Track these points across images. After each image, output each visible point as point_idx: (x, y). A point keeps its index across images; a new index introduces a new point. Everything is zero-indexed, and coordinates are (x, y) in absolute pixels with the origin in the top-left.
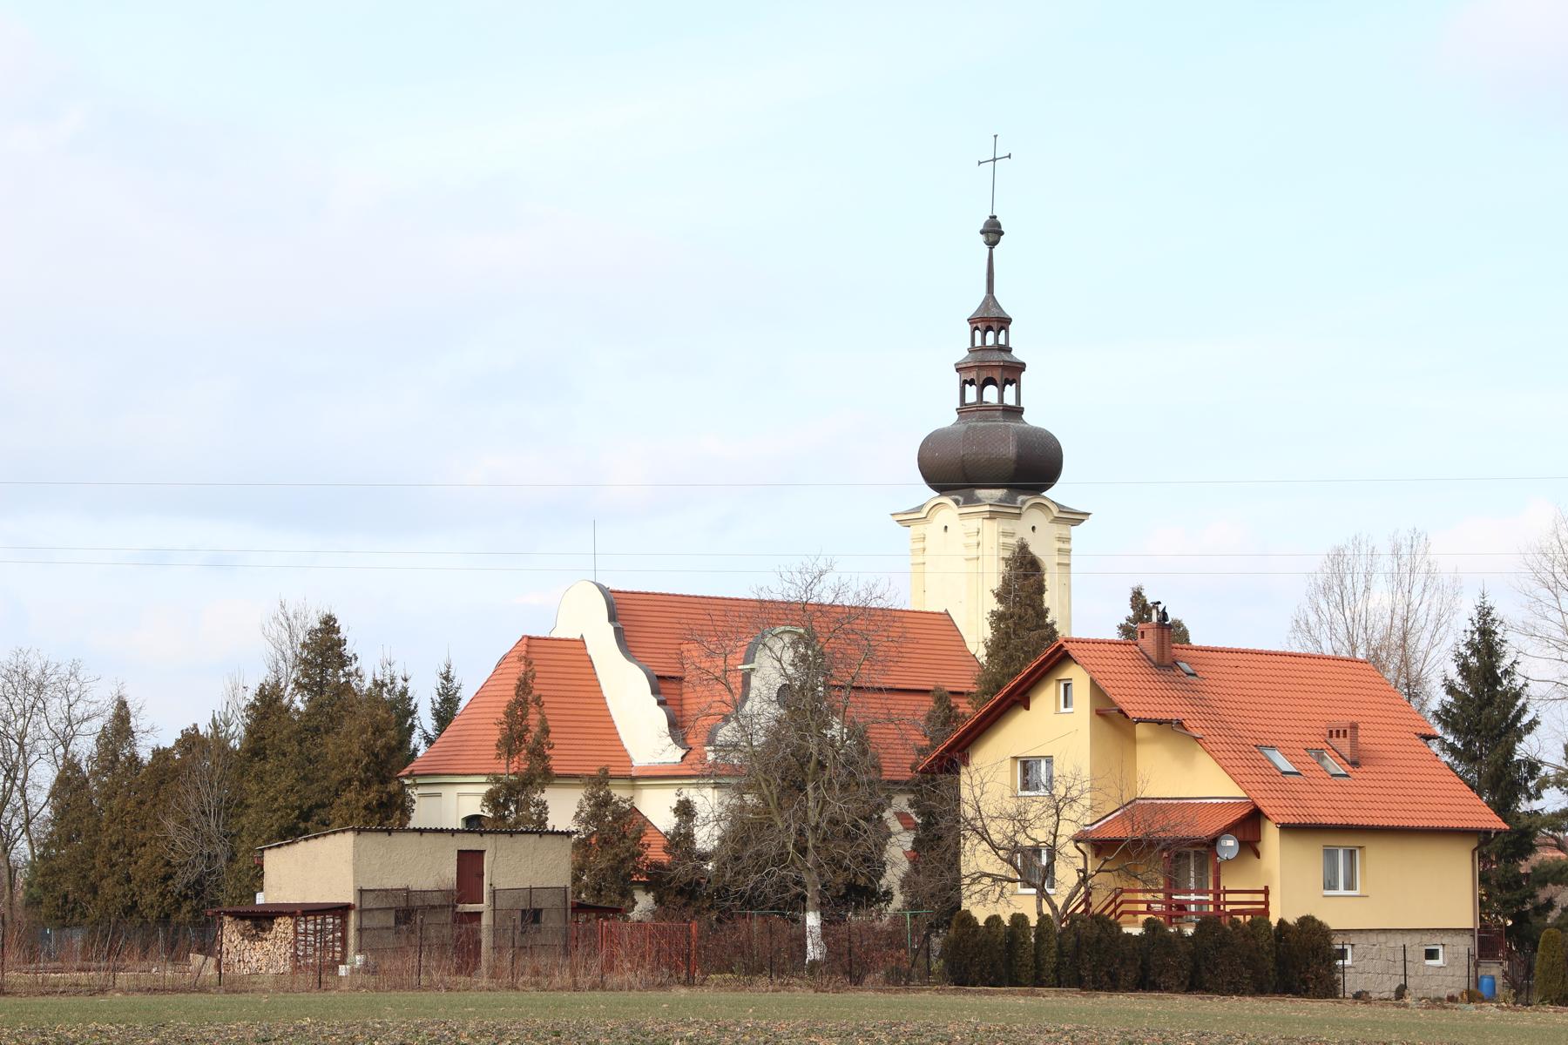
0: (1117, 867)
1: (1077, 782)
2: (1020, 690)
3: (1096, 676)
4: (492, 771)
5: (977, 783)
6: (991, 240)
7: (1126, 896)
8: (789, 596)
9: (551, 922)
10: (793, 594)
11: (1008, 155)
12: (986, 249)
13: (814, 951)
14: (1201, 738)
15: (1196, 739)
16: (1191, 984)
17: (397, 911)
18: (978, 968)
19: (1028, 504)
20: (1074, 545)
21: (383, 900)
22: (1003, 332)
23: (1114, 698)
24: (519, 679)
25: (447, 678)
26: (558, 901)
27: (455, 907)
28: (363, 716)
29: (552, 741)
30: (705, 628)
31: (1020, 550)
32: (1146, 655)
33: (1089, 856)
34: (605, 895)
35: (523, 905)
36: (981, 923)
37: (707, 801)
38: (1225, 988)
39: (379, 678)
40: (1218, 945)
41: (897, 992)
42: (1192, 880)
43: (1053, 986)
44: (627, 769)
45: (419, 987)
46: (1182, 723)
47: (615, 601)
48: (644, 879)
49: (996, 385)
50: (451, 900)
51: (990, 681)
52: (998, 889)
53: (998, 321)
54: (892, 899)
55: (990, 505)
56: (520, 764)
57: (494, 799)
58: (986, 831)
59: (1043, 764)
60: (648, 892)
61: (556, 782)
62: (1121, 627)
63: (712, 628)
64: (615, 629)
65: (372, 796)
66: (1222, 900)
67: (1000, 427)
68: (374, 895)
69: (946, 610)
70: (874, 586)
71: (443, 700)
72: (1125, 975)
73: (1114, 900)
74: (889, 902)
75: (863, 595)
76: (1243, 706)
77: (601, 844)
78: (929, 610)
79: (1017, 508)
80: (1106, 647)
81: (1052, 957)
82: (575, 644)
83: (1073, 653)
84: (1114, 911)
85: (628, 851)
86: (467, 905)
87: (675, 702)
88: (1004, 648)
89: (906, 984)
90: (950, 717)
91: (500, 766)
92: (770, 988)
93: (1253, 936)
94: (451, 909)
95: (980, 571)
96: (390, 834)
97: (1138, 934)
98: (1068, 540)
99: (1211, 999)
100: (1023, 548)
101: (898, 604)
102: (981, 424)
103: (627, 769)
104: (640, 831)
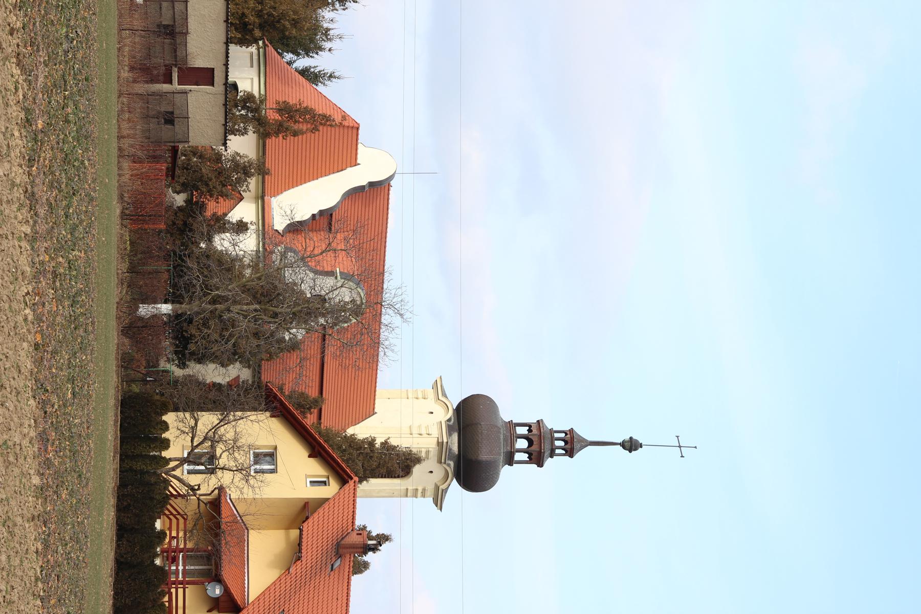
0: (201, 512)
1: (259, 483)
2: (322, 452)
3: (331, 501)
4: (268, 98)
5: (259, 418)
6: (626, 444)
7: (181, 521)
8: (386, 294)
9: (166, 132)
10: (387, 297)
11: (683, 455)
12: (620, 441)
13: (144, 310)
14: (289, 573)
15: (289, 569)
16: (122, 563)
17: (173, 26)
18: (133, 415)
19: (448, 469)
20: (420, 499)
21: (180, 16)
22: (564, 452)
23: (316, 514)
24: (330, 116)
25: (331, 76)
26: (180, 137)
27: (176, 65)
28: (305, 13)
29: (288, 138)
30: (365, 236)
31: (416, 458)
32: (345, 536)
33: (208, 497)
34: (184, 172)
35: (177, 112)
36: (164, 418)
37: (249, 243)
38: (119, 586)
39: (331, 32)
40: (148, 581)
41: (117, 359)
42: (192, 567)
43: (120, 467)
44: (269, 194)
45: (121, 30)
46: (299, 560)
47: (383, 186)
48: (194, 200)
49: (528, 447)
50: (180, 63)
51: (328, 437)
52: (187, 430)
53: (571, 448)
54: (181, 368)
55: (447, 442)
56: (273, 116)
57: (249, 99)
58: (226, 424)
59: (272, 467)
60: (185, 202)
61: (260, 140)
62: (365, 527)
63: (365, 241)
64: (364, 186)
65: (251, 18)
66: (179, 586)
67: (500, 450)
68: (184, 11)
69: (376, 413)
70: (393, 351)
71: (316, 74)
72: (128, 517)
73: (179, 514)
74: (178, 366)
75: (387, 343)
76: (311, 603)
77: (218, 170)
78: (376, 401)
79: (445, 461)
80: (351, 509)
81: (140, 467)
82: (372, 409)
83: (347, 486)
84: (172, 514)
85: (214, 187)
86: (177, 74)
87: (314, 227)
88: (350, 446)
89: (122, 366)
90: (304, 408)
91: (271, 104)
92: (120, 271)
93: (153, 606)
94: (174, 63)
95: (403, 436)
96: (225, 21)
97: (156, 526)
98: (423, 496)
99: (111, 576)
100: (418, 460)
101: (381, 366)
102: (502, 437)
103: (269, 194)
104: (227, 196)
